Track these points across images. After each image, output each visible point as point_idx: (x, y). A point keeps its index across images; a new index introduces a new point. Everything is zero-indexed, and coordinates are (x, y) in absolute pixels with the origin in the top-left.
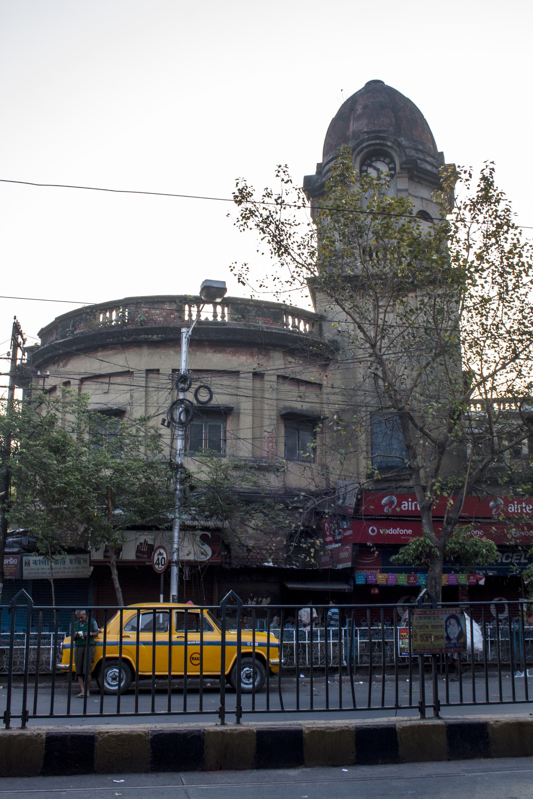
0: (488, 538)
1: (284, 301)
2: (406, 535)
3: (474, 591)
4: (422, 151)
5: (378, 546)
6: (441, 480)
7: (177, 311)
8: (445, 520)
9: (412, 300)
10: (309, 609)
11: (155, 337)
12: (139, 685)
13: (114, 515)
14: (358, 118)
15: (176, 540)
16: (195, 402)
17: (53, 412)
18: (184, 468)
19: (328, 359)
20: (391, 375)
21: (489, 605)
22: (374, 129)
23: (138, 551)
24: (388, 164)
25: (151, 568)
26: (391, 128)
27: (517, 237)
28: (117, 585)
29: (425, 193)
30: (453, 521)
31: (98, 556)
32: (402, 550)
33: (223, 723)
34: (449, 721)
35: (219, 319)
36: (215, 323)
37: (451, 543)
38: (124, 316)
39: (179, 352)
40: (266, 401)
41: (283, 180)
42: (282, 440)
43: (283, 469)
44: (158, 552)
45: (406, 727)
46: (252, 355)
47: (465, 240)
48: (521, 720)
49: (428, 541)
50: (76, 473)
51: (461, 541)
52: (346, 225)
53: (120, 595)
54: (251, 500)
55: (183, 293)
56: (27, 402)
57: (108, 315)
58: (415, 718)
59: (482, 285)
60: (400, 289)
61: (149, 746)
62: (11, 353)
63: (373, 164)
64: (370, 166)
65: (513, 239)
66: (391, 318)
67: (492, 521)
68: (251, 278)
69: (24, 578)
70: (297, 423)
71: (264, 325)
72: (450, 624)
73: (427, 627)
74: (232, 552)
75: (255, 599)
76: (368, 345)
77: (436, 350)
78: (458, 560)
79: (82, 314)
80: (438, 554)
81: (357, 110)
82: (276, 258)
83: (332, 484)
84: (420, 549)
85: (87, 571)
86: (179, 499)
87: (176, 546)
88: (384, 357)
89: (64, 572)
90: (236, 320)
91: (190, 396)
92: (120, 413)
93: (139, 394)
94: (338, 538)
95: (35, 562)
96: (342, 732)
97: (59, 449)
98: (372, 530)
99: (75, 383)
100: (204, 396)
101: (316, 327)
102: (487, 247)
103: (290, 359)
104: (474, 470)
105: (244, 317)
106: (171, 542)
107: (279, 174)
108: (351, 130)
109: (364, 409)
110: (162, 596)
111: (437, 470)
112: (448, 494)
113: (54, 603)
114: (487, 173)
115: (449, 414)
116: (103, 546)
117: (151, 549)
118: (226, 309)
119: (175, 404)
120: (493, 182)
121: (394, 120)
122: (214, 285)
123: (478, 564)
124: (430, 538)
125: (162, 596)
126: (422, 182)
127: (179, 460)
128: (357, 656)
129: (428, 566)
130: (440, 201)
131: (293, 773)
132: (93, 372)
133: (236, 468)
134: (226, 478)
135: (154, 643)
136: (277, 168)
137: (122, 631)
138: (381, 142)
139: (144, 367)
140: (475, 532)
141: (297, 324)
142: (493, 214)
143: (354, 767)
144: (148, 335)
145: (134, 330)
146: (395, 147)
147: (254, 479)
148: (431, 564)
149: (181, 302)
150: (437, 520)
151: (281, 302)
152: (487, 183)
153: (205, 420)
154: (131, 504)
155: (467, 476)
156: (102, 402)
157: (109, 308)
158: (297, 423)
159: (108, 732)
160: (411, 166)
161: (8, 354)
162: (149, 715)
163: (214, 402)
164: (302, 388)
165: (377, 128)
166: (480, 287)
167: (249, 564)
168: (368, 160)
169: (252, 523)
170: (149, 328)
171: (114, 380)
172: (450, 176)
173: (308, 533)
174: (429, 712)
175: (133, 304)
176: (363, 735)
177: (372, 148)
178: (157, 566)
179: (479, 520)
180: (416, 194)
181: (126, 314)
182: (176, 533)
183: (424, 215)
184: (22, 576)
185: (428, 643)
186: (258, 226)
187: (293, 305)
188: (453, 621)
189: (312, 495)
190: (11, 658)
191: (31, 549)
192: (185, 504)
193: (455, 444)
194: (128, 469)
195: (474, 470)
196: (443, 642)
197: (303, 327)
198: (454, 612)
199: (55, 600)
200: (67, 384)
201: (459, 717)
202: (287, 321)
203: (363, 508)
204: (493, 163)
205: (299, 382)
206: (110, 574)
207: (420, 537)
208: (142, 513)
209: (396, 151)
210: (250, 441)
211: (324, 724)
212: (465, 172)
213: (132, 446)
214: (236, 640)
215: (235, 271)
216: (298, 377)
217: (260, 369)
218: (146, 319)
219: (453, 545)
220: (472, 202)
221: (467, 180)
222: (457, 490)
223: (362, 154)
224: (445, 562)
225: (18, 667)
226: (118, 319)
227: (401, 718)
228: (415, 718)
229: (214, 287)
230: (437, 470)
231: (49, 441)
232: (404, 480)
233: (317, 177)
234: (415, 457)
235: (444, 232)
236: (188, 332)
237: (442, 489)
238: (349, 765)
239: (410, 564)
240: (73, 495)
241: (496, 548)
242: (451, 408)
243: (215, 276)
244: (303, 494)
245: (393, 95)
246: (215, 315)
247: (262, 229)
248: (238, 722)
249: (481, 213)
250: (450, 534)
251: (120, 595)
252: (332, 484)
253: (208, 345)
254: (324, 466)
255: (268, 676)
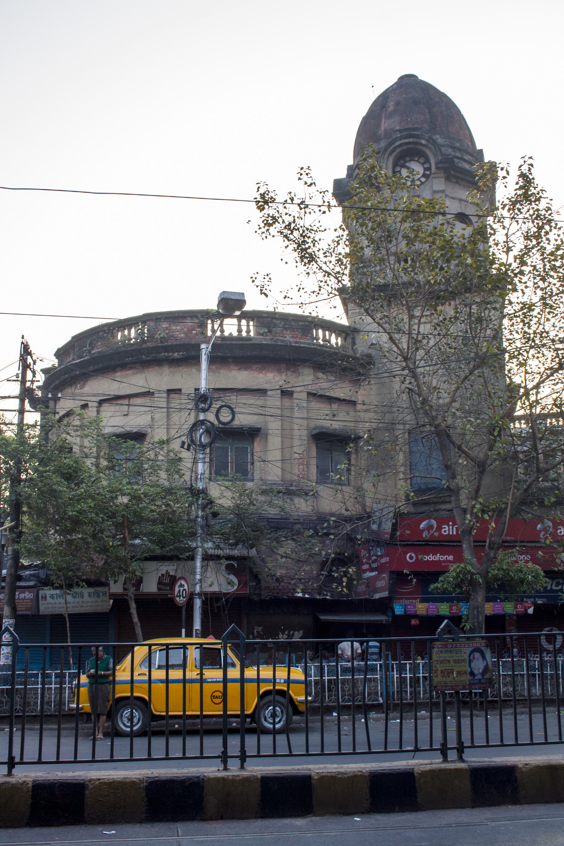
0: (534, 563)
1: (310, 313)
2: (447, 561)
3: (522, 620)
4: (459, 150)
5: (416, 574)
6: (482, 501)
7: (200, 327)
8: (487, 544)
9: (449, 310)
10: (350, 643)
11: (176, 354)
12: (157, 726)
13: (133, 545)
14: (390, 116)
15: (198, 570)
16: (216, 423)
17: (64, 436)
18: (206, 494)
19: (359, 374)
20: (425, 389)
21: (539, 636)
22: (407, 127)
23: (160, 583)
24: (423, 164)
25: (172, 601)
26: (426, 126)
27: (561, 237)
28: (136, 619)
29: (463, 194)
30: (496, 546)
31: (116, 588)
32: (441, 579)
33: (226, 769)
34: (473, 764)
35: (244, 334)
36: (240, 338)
37: (494, 570)
38: (143, 333)
39: (199, 371)
40: (296, 421)
41: (306, 183)
42: (314, 462)
43: (312, 493)
44: (179, 584)
45: (425, 771)
46: (279, 371)
47: (504, 242)
48: (553, 763)
49: (469, 568)
50: (89, 501)
51: (505, 567)
52: (373, 229)
53: (138, 630)
54: (281, 526)
55: (205, 308)
56: (46, 428)
57: (126, 332)
58: (437, 761)
59: (522, 290)
60: (435, 297)
61: (144, 794)
62: (20, 375)
63: (407, 164)
64: (403, 166)
65: (556, 240)
66: (425, 329)
67: (539, 545)
68: (274, 289)
69: (41, 613)
70: (329, 442)
71: (291, 340)
72: (474, 658)
73: (449, 661)
74: (262, 582)
75: (286, 633)
76: (400, 358)
77: (475, 361)
78: (502, 588)
79: (99, 332)
80: (480, 580)
81: (389, 106)
82: (302, 268)
83: (368, 510)
84: (461, 575)
85: (105, 605)
86: (201, 527)
87: (198, 577)
88: (419, 370)
89: (83, 606)
90: (262, 335)
91: (211, 417)
92: (139, 437)
93: (160, 416)
94: (374, 565)
95: (52, 596)
96: (355, 778)
97: (71, 475)
98: (410, 557)
99: (93, 405)
100: (225, 417)
101: (349, 340)
102: (527, 250)
103: (320, 375)
104: (518, 490)
105: (270, 331)
106: (194, 573)
107: (301, 177)
108: (383, 128)
109: (401, 427)
110: (183, 631)
111: (477, 491)
112: (489, 516)
113: (69, 640)
114: (525, 169)
115: (489, 431)
116: (122, 578)
117: (173, 580)
118: (251, 323)
119: (197, 424)
120: (533, 179)
121: (428, 117)
122: (232, 297)
123: (524, 592)
124: (471, 564)
125: (183, 631)
126: (460, 182)
127: (200, 485)
128: (393, 692)
129: (470, 595)
130: (476, 201)
131: (299, 822)
132: (112, 393)
133: (264, 492)
134: (251, 503)
135: (167, 681)
136: (299, 170)
137: (140, 668)
138: (415, 140)
139: (165, 388)
140: (522, 557)
141: (327, 337)
142: (534, 214)
143: (368, 816)
144: (168, 352)
145: (153, 347)
146: (430, 146)
147: (281, 503)
148: (473, 592)
149: (203, 316)
150: (479, 545)
151: (306, 314)
152: (526, 180)
153: (230, 442)
154: (152, 533)
155: (510, 498)
156: (118, 424)
157: (128, 325)
158: (329, 442)
159: (99, 779)
160: (447, 165)
161: (17, 376)
162: (145, 760)
163: (236, 423)
164: (335, 406)
165: (410, 126)
166: (520, 294)
167: (280, 594)
168: (401, 160)
169: (281, 551)
170: (169, 346)
171: (134, 401)
172: (485, 174)
173: (341, 561)
174: (452, 755)
175: (152, 320)
176: (378, 780)
177: (405, 147)
178: (178, 599)
179: (523, 544)
180: (454, 196)
181: (146, 331)
182: (198, 563)
183: (462, 218)
184: (38, 611)
185: (450, 679)
186: (282, 233)
187: (320, 317)
188: (477, 655)
189: (346, 521)
190: (25, 698)
191: (46, 583)
192: (209, 532)
193: (497, 463)
194: (146, 495)
195: (518, 490)
196: (466, 678)
197: (335, 340)
198: (478, 645)
199: (71, 636)
200: (85, 406)
201: (486, 759)
202: (317, 334)
203: (398, 534)
204: (531, 158)
205: (331, 400)
206: (129, 608)
207: (461, 563)
208: (161, 543)
209: (430, 149)
210: (279, 464)
211: (336, 768)
212: (502, 169)
213: (149, 471)
214: (239, 677)
215: (257, 282)
216: (327, 394)
217: (287, 386)
218: (166, 336)
219: (496, 572)
220: (510, 201)
221: (504, 178)
222: (500, 512)
223: (395, 153)
224: (489, 589)
225: (32, 707)
226: (138, 335)
227: (421, 761)
228: (437, 761)
229: (232, 299)
230: (477, 491)
231: (60, 467)
232: (444, 503)
233: (347, 180)
234: (454, 477)
235: (482, 234)
236: (207, 348)
237: (483, 512)
238: (363, 813)
239: (450, 593)
240: (86, 523)
241: (542, 574)
242: (491, 424)
243: (233, 287)
244: (333, 519)
245: (427, 88)
246: (240, 331)
247: (286, 236)
248: (242, 767)
249: (521, 213)
250: (493, 560)
251: (138, 630)
252: (368, 510)
253: (233, 362)
254: (359, 489)
255: (297, 715)
